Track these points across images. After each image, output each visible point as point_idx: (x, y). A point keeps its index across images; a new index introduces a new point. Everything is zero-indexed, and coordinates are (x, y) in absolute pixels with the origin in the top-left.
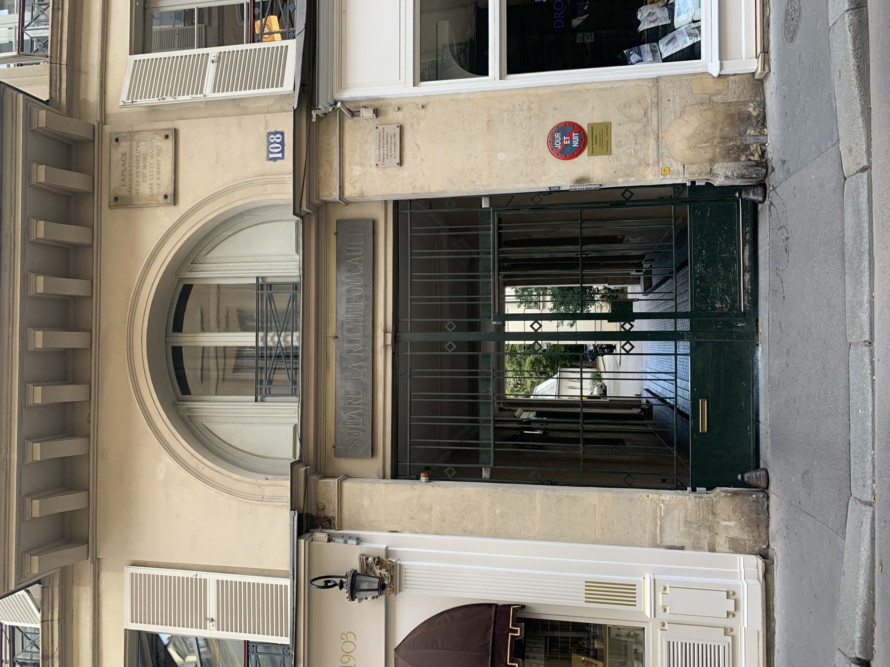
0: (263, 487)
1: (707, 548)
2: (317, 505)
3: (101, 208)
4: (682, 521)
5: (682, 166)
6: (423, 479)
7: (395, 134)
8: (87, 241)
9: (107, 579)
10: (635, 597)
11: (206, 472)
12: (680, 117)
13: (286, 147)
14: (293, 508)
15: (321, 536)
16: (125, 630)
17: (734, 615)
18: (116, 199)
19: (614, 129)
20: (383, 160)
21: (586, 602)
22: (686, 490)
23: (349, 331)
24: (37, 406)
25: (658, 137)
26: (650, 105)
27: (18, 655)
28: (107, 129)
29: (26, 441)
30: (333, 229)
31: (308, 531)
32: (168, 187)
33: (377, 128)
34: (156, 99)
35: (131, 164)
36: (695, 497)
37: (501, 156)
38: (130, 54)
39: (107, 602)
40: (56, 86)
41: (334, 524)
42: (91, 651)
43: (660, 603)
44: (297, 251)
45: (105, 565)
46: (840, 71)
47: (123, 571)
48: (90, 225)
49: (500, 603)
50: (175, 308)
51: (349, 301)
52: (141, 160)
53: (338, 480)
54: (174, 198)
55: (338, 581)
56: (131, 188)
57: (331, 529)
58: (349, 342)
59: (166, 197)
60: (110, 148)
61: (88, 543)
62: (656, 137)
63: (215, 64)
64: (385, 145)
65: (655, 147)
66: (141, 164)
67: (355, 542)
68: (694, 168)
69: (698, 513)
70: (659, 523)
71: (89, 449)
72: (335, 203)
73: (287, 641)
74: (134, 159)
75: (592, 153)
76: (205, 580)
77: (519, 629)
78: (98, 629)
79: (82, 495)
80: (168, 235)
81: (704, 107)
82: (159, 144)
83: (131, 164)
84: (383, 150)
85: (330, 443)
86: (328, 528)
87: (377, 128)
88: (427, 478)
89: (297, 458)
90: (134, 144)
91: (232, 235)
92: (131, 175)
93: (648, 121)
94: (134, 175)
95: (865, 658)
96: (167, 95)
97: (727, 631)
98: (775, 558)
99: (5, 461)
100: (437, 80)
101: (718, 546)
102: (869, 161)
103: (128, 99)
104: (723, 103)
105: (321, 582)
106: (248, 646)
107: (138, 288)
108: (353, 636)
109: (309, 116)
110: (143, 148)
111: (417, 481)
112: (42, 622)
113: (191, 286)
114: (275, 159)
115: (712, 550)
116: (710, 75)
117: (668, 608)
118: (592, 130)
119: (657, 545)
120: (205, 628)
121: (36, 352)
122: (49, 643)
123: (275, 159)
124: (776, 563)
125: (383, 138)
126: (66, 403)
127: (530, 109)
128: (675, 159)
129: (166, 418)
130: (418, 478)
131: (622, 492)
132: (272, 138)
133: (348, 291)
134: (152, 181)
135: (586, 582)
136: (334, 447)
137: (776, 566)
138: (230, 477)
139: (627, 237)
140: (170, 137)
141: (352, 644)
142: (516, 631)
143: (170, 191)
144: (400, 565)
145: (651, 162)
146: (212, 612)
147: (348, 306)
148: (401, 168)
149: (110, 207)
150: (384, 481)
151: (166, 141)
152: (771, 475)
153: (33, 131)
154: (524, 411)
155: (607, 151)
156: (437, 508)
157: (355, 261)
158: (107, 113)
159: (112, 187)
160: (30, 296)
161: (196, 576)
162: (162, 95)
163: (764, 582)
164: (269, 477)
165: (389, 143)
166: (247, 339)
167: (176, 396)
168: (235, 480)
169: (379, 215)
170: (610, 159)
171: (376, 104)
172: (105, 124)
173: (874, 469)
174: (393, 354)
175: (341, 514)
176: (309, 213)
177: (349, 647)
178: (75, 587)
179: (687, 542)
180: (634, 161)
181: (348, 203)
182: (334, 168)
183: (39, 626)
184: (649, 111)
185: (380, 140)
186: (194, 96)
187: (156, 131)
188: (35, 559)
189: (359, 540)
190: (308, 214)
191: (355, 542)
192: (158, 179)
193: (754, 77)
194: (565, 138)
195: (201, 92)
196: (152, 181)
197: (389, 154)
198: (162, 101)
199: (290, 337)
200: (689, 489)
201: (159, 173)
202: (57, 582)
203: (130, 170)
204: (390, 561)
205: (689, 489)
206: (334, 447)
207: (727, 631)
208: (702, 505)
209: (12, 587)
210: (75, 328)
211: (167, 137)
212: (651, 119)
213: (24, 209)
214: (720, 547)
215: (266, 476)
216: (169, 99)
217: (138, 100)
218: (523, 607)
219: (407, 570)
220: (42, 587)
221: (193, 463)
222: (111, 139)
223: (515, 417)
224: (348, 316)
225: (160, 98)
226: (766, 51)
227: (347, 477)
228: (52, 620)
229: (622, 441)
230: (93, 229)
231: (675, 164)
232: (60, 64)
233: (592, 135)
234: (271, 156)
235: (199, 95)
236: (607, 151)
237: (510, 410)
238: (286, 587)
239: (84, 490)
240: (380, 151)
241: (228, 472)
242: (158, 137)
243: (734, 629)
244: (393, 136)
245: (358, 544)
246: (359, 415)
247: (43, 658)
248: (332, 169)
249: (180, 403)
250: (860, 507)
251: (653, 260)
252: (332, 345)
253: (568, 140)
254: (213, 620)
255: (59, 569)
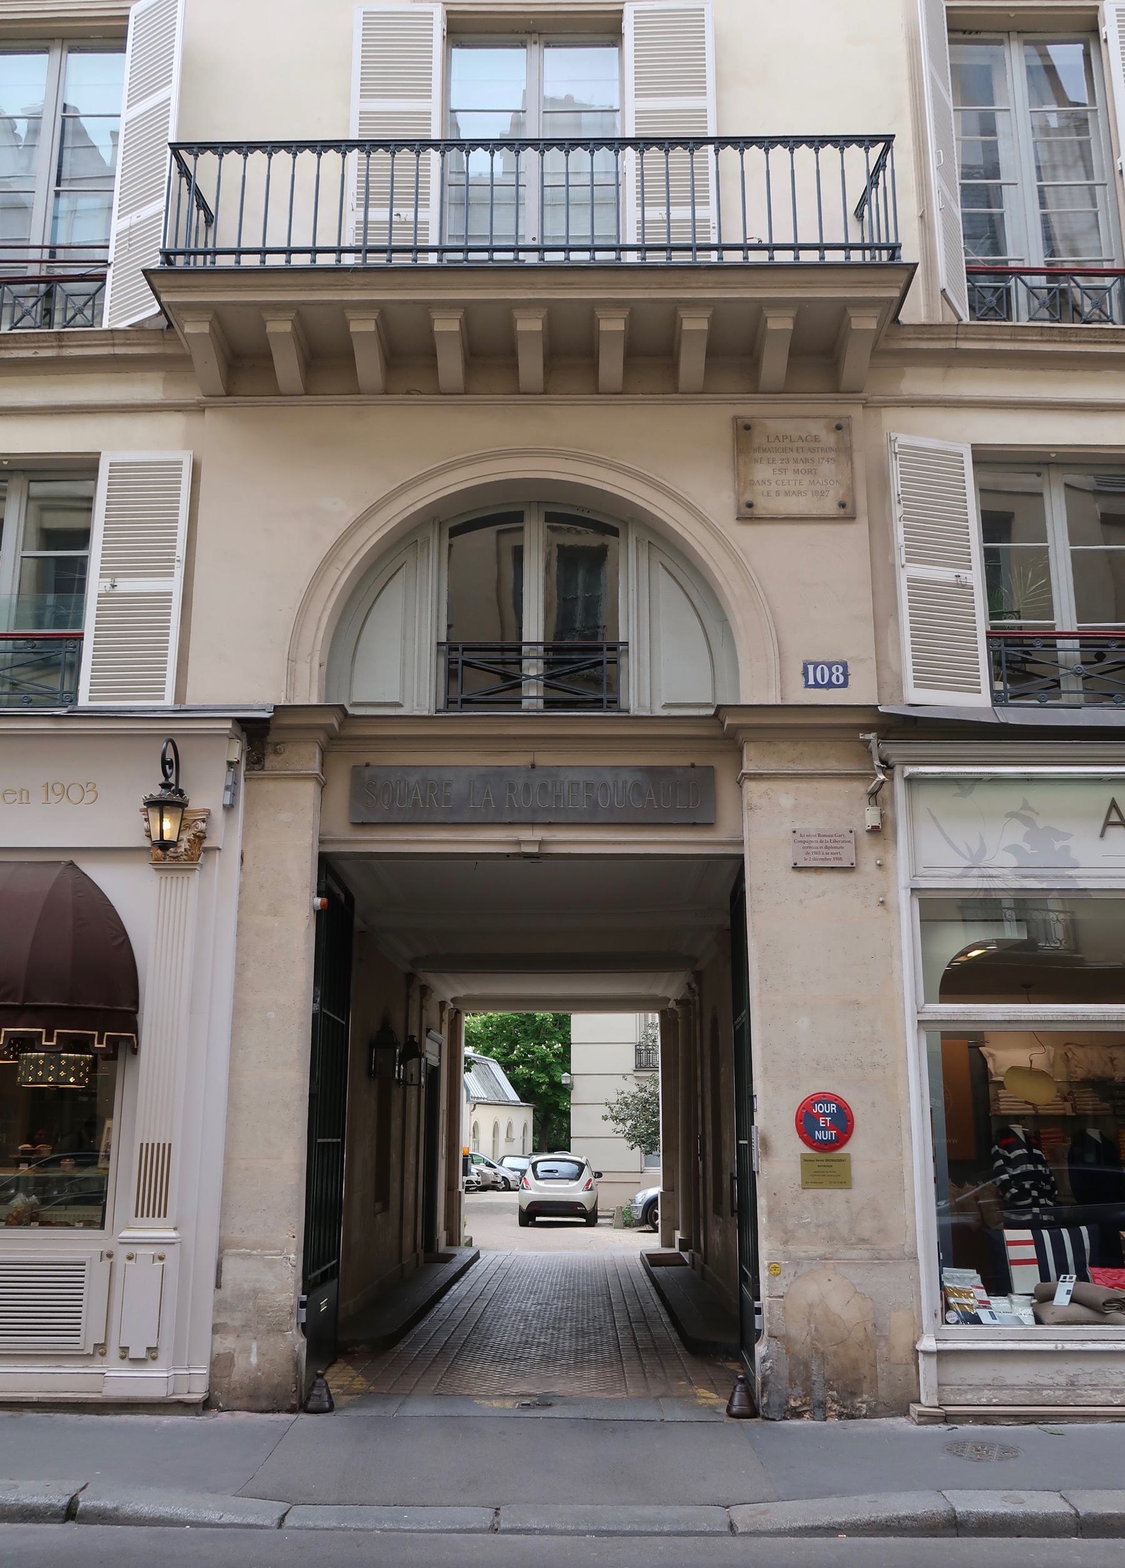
0: (308, 661)
1: (219, 1321)
2: (283, 743)
3: (734, 404)
4: (258, 1285)
5: (781, 1294)
6: (318, 901)
7: (840, 859)
8: (683, 384)
9: (175, 424)
10: (142, 1216)
11: (333, 573)
12: (856, 1292)
13: (823, 691)
14: (278, 709)
15: (236, 751)
16: (100, 453)
17: (123, 1358)
18: (747, 428)
19: (840, 1194)
20: (801, 841)
21: (142, 1144)
22: (303, 1294)
23: (543, 786)
24: (430, 323)
25: (826, 1259)
26: (876, 1247)
27: (61, 287)
28: (856, 412)
29: (379, 310)
30: (700, 762)
31: (243, 730)
32: (764, 508)
33: (851, 832)
34: (900, 489)
35: (800, 450)
36: (292, 1306)
37: (804, 1023)
38: (973, 445)
39: (141, 427)
40: (923, 333)
41: (254, 769)
42: (68, 404)
43: (140, 1251)
44: (667, 706)
45: (195, 421)
46: (876, 1501)
47: (186, 448)
48: (706, 390)
49: (139, 1017)
50: (583, 515)
51: (589, 786)
52: (807, 466)
53: (316, 774)
54: (748, 514)
55: (172, 780)
56: (764, 450)
57: (247, 765)
58: (527, 787)
59: (750, 505)
60: (826, 417)
61: (228, 395)
62: (828, 1256)
63: (953, 580)
64: (823, 845)
65: (811, 1254)
66: (801, 466)
67: (228, 803)
68: (778, 1312)
69: (270, 1310)
70: (255, 1252)
71: (368, 394)
72: (740, 765)
73: (83, 701)
74: (809, 455)
75: (805, 1160)
76: (171, 575)
77: (104, 1046)
78: (100, 412)
79: (299, 386)
80: (690, 508)
81: (870, 1328)
82: (832, 493)
83: (800, 450)
84: (817, 842)
85: (371, 758)
86: (247, 759)
87: (851, 832)
88: (320, 908)
89: (351, 711)
90: (833, 455)
91: (693, 605)
92: (784, 450)
93: (852, 1244)
94: (785, 456)
95: (78, 1513)
96: (905, 506)
97: (101, 1349)
98: (205, 1417)
99: (348, 283)
100: (921, 921)
101: (221, 1338)
102: (743, 1534)
103: (900, 446)
104: (875, 1356)
105: (170, 756)
106: (75, 639)
107: (610, 465)
108: (93, 799)
109: (867, 729)
110: (827, 469)
111: (315, 893)
112: (112, 331)
113: (618, 536)
114: (805, 674)
115: (216, 1329)
116: (919, 1338)
117: (132, 1262)
118: (840, 1161)
119: (223, 1250)
120: (102, 576)
121: (511, 323)
122: (81, 341)
123: (805, 674)
124: (197, 1418)
125: (835, 841)
126: (434, 355)
127: (874, 1065)
128: (792, 1283)
129: (413, 509)
130: (319, 895)
131: (346, 202)
132: (837, 670)
133: (605, 785)
134: (774, 484)
135: (170, 1145)
136: (368, 765)
137: (194, 1419)
138: (324, 609)
139: (721, 1220)
140: (842, 511)
141: (79, 800)
142: (100, 1042)
143: (758, 511)
144: (196, 869)
145: (790, 1248)
146: (126, 585)
147: (581, 785)
148: (790, 869)
149: (735, 419)
150: (316, 844)
151: (836, 505)
152: (322, 1416)
153: (845, 310)
154: (440, 1046)
155: (806, 1185)
156: (276, 925)
157: (650, 795)
158: (883, 409)
159: (767, 421)
160: (594, 312)
161: (178, 561)
162: (905, 499)
163: (172, 1401)
164: (324, 668)
165: (827, 851)
166: (534, 628)
167: (447, 520)
168: (320, 618)
169: (722, 833)
170: (796, 1187)
171: (888, 830)
172: (863, 407)
173: (327, 1529)
174: (508, 855)
175: (268, 779)
176: (723, 726)
177: (75, 794)
178: (161, 374)
179: (227, 1292)
180: (791, 1223)
181: (740, 784)
182: (791, 765)
183: (106, 325)
184: (868, 1246)
185: (832, 836)
186: (903, 549)
187: (851, 489)
188: (205, 328)
189: (229, 808)
190: (722, 723)
191: (227, 802)
192: (778, 493)
193: (913, 1402)
194: (828, 1119)
195: (907, 562)
196: (774, 484)
197: (811, 851)
198: (897, 499)
199: (535, 694)
200: (304, 1298)
201: (787, 494)
202: (169, 350)
203: (792, 450)
204: (199, 855)
205: (304, 1298)
206: (368, 765)
207: (101, 1349)
208: (280, 1316)
209: (165, 298)
210: (548, 369)
211: (843, 505)
212: (855, 1249)
213: (726, 300)
214: (219, 1340)
215: (326, 663)
216: (898, 511)
217: (899, 462)
218: (135, 1051)
219: (186, 879)
220: (162, 330)
221: (347, 553)
222: (840, 418)
223: (428, 1030)
224: (566, 785)
225: (901, 496)
226: (949, 1418)
227: (323, 786)
228: (114, 345)
229: (386, 1208)
230: (702, 393)
231: (785, 1283)
232: (957, 339)
233: (832, 1160)
234: (811, 668)
235: (904, 557)
236: (806, 1185)
237: (442, 1020)
238: (162, 698)
239: (306, 389)
240: (815, 836)
241: (331, 607)
242: (841, 492)
243: (104, 1358)
244: (838, 856)
245: (224, 806)
246: (415, 802)
247: (59, 333)
248: (789, 762)
249: (437, 529)
250: (277, 1515)
251: (693, 1268)
252: (521, 760)
253: (826, 1123)
254: (114, 586)
255: (188, 353)
